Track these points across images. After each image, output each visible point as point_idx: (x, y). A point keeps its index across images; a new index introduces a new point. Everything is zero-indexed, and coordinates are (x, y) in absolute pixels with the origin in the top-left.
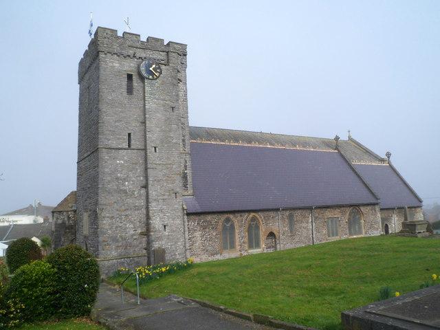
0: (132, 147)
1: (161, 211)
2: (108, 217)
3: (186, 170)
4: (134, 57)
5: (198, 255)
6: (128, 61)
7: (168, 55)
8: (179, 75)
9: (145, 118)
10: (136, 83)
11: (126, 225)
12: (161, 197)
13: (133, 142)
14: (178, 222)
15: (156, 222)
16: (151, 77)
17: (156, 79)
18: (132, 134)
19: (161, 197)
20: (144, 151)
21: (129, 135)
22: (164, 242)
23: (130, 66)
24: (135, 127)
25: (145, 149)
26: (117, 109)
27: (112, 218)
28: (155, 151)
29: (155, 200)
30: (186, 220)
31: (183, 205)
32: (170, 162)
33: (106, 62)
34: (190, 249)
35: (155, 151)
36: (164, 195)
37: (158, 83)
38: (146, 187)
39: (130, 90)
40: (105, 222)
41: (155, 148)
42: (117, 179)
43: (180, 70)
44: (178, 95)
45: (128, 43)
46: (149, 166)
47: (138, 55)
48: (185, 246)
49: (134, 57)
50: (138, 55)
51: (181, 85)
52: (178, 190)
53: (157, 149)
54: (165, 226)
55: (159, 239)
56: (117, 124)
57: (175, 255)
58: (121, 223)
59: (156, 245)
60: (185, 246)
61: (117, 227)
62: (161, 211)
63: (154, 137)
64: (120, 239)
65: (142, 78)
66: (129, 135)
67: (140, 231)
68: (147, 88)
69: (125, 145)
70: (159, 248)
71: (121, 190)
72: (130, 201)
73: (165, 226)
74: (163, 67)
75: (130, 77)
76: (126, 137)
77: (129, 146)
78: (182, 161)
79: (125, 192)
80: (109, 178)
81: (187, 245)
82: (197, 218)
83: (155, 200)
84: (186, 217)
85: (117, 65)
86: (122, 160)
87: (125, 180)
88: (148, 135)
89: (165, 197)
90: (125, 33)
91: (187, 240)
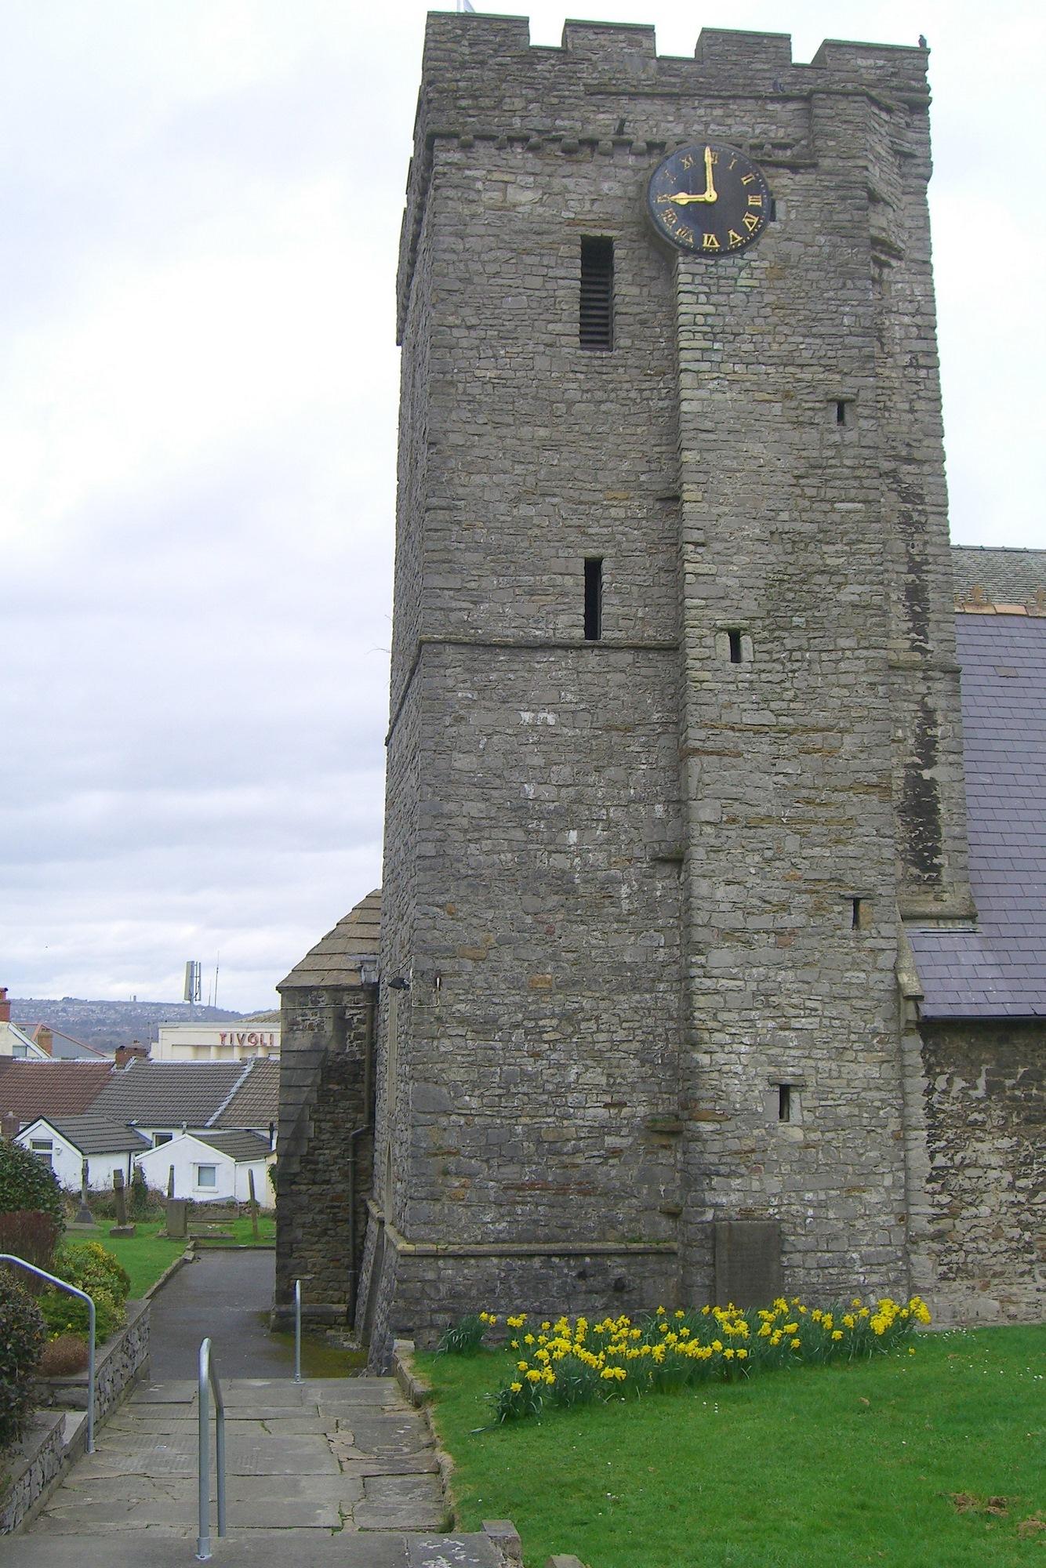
0: (606, 635)
1: (764, 997)
2: (463, 1021)
3: (930, 763)
4: (623, 143)
5: (986, 1277)
6: (586, 168)
7: (809, 114)
8: (880, 221)
9: (671, 429)
10: (627, 288)
11: (561, 1067)
12: (764, 921)
13: (610, 606)
14: (867, 1069)
15: (734, 1067)
16: (709, 241)
17: (740, 250)
18: (606, 565)
19: (764, 921)
20: (661, 664)
21: (593, 568)
22: (774, 1184)
23: (594, 194)
24: (621, 529)
25: (673, 649)
26: (526, 431)
27: (486, 1026)
28: (736, 656)
29: (729, 934)
30: (915, 1059)
31: (895, 970)
32: (822, 718)
33: (467, 185)
34: (939, 1236)
35: (736, 656)
36: (784, 907)
37: (749, 272)
38: (676, 860)
39: (596, 326)
40: (446, 1045)
41: (735, 636)
42: (521, 810)
43: (883, 189)
44: (878, 333)
45: (589, 76)
46: (696, 736)
47: (640, 134)
48: (903, 1218)
49: (623, 143)
50: (640, 134)
51: (897, 275)
52: (871, 878)
53: (746, 642)
54: (785, 1091)
55: (752, 1159)
56: (524, 510)
57: (845, 1265)
58: (536, 1055)
59: (728, 1197)
60: (903, 1218)
61: (507, 1083)
62: (764, 997)
63: (726, 575)
64: (529, 1147)
65: (663, 252)
66: (593, 568)
67: (642, 1110)
68: (688, 306)
69: (570, 623)
70: (747, 1214)
71: (540, 875)
72: (589, 937)
73: (785, 1091)
74: (782, 180)
75: (596, 257)
76: (576, 584)
77: (592, 626)
78: (908, 709)
79: (562, 883)
80: (475, 808)
81: (923, 1209)
82: (987, 1059)
83: (729, 934)
84: (914, 1042)
85: (529, 196)
86: (552, 706)
87: (565, 817)
88: (696, 564)
89: (794, 920)
90: (572, 26)
91: (917, 1183)
